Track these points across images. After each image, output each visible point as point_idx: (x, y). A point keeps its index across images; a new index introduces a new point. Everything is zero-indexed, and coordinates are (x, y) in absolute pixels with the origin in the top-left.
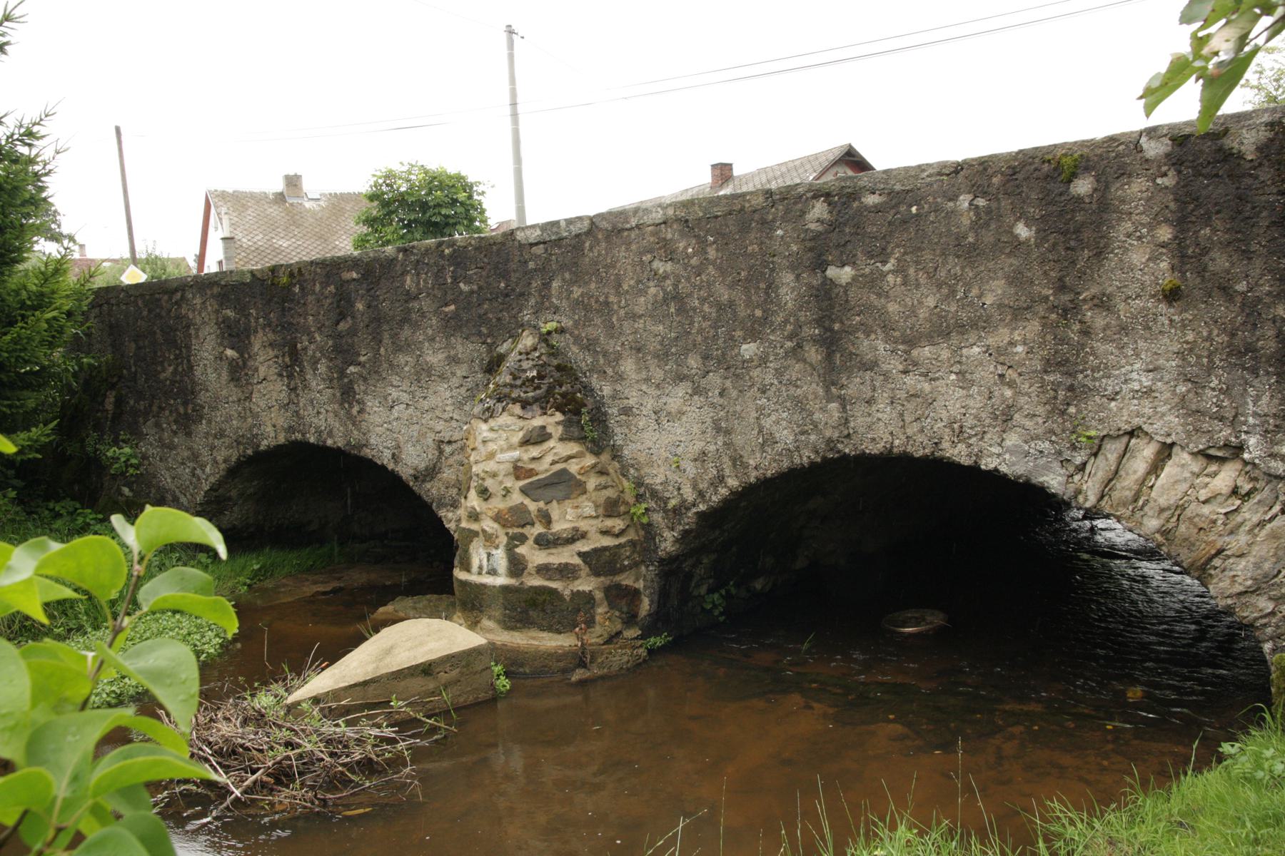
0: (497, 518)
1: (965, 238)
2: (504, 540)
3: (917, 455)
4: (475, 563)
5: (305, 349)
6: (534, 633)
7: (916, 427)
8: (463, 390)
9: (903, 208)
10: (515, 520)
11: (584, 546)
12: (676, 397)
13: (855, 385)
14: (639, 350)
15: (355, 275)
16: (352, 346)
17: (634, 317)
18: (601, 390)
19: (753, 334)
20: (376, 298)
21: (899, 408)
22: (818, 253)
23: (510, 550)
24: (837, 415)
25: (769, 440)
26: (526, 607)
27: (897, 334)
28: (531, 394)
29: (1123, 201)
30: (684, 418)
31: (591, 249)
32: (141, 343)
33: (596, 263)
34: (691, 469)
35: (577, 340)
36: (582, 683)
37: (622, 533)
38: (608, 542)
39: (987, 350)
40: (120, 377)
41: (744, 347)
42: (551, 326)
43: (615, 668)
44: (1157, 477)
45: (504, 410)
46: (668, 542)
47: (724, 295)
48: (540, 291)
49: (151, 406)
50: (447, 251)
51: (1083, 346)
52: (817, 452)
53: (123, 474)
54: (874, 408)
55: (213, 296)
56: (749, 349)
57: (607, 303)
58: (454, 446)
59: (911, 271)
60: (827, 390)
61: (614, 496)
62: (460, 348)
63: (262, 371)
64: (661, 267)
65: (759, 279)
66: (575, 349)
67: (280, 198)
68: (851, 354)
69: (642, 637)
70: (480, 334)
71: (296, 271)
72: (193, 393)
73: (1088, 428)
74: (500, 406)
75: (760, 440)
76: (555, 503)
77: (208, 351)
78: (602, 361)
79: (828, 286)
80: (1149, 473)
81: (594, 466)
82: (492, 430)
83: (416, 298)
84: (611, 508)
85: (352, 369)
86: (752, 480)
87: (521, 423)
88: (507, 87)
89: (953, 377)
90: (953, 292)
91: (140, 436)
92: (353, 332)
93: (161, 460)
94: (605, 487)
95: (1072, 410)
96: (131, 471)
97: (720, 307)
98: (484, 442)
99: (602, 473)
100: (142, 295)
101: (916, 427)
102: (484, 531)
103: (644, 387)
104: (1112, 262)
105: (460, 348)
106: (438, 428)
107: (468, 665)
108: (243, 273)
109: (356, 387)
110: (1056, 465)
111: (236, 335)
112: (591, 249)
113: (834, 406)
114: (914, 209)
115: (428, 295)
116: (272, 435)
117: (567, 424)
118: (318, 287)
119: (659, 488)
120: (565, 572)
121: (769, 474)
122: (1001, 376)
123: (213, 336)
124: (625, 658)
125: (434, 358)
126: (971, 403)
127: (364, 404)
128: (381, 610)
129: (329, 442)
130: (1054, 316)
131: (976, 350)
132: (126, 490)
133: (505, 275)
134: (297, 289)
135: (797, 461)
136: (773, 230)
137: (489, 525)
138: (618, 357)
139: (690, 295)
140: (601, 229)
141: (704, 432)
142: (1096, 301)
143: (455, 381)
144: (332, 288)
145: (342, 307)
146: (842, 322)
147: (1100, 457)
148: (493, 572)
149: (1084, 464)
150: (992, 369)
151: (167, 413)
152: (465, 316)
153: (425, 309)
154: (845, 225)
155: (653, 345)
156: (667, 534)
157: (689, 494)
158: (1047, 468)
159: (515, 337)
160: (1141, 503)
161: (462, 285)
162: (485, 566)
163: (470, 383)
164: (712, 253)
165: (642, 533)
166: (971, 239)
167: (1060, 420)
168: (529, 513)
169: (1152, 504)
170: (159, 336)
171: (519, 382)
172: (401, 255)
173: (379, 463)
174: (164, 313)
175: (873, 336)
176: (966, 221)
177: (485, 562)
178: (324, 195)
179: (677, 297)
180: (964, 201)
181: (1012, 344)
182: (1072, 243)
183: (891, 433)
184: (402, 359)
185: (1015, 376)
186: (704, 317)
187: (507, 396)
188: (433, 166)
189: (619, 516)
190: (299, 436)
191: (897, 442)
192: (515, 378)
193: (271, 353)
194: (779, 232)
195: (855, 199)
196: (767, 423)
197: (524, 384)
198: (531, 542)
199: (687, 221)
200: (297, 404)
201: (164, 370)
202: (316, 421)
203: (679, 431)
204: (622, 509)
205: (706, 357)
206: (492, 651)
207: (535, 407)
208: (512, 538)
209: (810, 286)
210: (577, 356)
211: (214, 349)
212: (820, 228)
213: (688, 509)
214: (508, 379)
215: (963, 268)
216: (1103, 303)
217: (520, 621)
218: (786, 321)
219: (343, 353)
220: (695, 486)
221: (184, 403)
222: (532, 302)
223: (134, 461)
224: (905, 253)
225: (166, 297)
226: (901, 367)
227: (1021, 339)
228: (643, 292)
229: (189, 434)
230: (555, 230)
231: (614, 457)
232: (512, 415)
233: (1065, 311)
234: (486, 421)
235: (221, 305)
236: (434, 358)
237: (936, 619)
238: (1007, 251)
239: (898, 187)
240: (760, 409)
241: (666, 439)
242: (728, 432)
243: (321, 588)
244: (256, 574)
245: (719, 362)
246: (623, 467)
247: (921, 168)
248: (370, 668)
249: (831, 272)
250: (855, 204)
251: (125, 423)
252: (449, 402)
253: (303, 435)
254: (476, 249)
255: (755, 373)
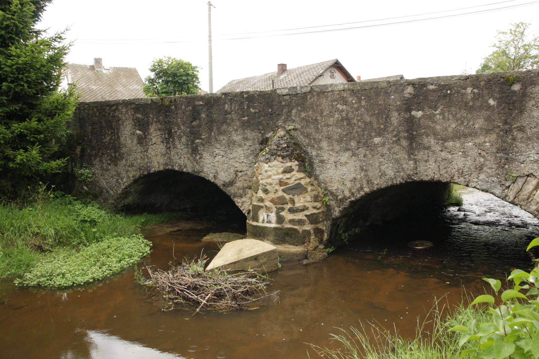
0: (272, 201)
1: (469, 103)
2: (275, 210)
3: (443, 181)
4: (261, 218)
5: (176, 132)
6: (287, 246)
7: (444, 171)
8: (249, 151)
9: (444, 91)
10: (280, 202)
11: (308, 213)
12: (345, 157)
13: (421, 155)
14: (329, 138)
15: (201, 103)
16: (199, 131)
17: (328, 126)
18: (311, 153)
19: (379, 134)
20: (211, 113)
21: (438, 164)
22: (408, 106)
23: (278, 214)
24: (412, 166)
25: (383, 174)
26: (283, 235)
27: (439, 137)
28: (285, 153)
29: (532, 93)
30: (348, 165)
31: (310, 99)
32: (95, 127)
33: (312, 104)
34: (349, 185)
35: (302, 133)
36: (307, 265)
37: (320, 208)
38: (315, 211)
39: (475, 144)
40: (83, 140)
41: (375, 139)
42: (291, 127)
43: (318, 259)
44: (537, 191)
45: (275, 159)
46: (336, 212)
47: (368, 119)
48: (287, 114)
49: (98, 153)
50: (245, 96)
51: (512, 144)
52: (403, 179)
53: (85, 180)
54: (428, 163)
55: (131, 108)
56: (377, 140)
57: (316, 120)
58: (243, 173)
59: (446, 114)
60: (409, 156)
61: (317, 194)
62: (249, 134)
63: (154, 140)
64: (340, 107)
65: (383, 113)
66: (301, 137)
67: (92, 68)
68: (420, 143)
69: (325, 248)
70: (259, 129)
71: (173, 100)
72: (119, 148)
73: (512, 173)
74: (273, 158)
75: (380, 174)
76: (296, 196)
77: (127, 132)
78: (313, 142)
79: (412, 118)
80: (534, 190)
81: (310, 182)
82: (270, 166)
83: (230, 113)
84: (316, 198)
85: (198, 141)
86: (375, 189)
87: (282, 165)
88: (208, 28)
89: (461, 153)
90: (463, 122)
91: (93, 165)
92: (199, 126)
93: (101, 175)
94: (314, 190)
95: (507, 167)
96: (89, 179)
97: (366, 124)
98: (266, 171)
99: (312, 185)
100: (96, 107)
101: (444, 171)
102: (266, 206)
103: (331, 153)
104: (526, 115)
105: (249, 134)
106: (236, 166)
107: (270, 257)
108: (147, 99)
109: (199, 148)
110: (499, 186)
111: (142, 125)
112: (310, 99)
113: (411, 162)
114: (449, 92)
115: (236, 113)
116: (157, 166)
117: (300, 165)
118: (183, 107)
119: (334, 191)
120: (300, 222)
121: (382, 187)
122: (480, 154)
123: (131, 125)
124: (321, 256)
125: (237, 138)
126: (467, 163)
127: (202, 155)
128: (205, 238)
129: (185, 170)
130: (502, 133)
131: (470, 144)
132: (85, 188)
133: (271, 107)
134: (173, 107)
135: (395, 182)
136: (390, 96)
137: (268, 204)
138: (320, 140)
139: (353, 118)
140: (315, 91)
141: (355, 171)
142: (519, 128)
143: (246, 147)
144: (190, 108)
145: (195, 114)
146: (417, 131)
147: (516, 184)
148: (269, 222)
149: (509, 186)
150: (476, 151)
151: (106, 156)
152: (252, 122)
153: (234, 118)
154: (420, 96)
155: (336, 137)
156: (337, 209)
157: (347, 194)
158: (495, 187)
159: (275, 132)
160: (530, 200)
161: (251, 109)
162: (267, 219)
163: (252, 148)
164: (363, 103)
165: (326, 208)
166: (471, 104)
167: (502, 170)
168: (286, 199)
169: (534, 200)
170: (104, 123)
171: (280, 149)
172: (223, 96)
173: (207, 179)
174: (106, 115)
175: (429, 137)
176: (469, 97)
177: (266, 218)
178: (111, 68)
179: (347, 119)
180: (469, 90)
181: (485, 142)
182: (511, 107)
183: (434, 173)
184: (222, 137)
185: (485, 154)
186: (359, 127)
187: (276, 154)
188: (178, 59)
189: (318, 202)
190: (170, 167)
191: (436, 176)
192: (278, 147)
193: (159, 133)
194: (393, 97)
195: (424, 87)
196: (383, 168)
197: (282, 149)
198: (286, 210)
199: (353, 90)
200: (170, 154)
201: (105, 138)
202: (179, 161)
203: (345, 170)
204: (320, 199)
205: (359, 142)
206: (273, 252)
207: (287, 158)
208: (278, 209)
209: (404, 118)
210: (301, 139)
211: (130, 130)
212: (410, 96)
213: (346, 200)
214: (275, 147)
215: (467, 114)
216: (521, 129)
217: (281, 241)
218: (394, 130)
219: (194, 134)
220: (350, 191)
221: (115, 152)
222: (283, 117)
223: (90, 176)
224: (444, 108)
225: (108, 108)
226: (440, 149)
227: (489, 141)
228: (333, 116)
229: (116, 165)
230: (295, 90)
231: (316, 179)
232: (278, 161)
233: (506, 131)
234: (267, 163)
235: (135, 112)
236: (237, 138)
237: (429, 244)
238: (485, 109)
239: (442, 83)
240: (381, 163)
241: (339, 173)
242: (366, 171)
243: (172, 230)
244: (142, 224)
245: (364, 144)
246: (319, 183)
247: (452, 77)
248: (236, 257)
249: (413, 113)
250: (425, 88)
251: (85, 159)
252: (242, 155)
253: (172, 167)
254: (258, 96)
255: (379, 149)
